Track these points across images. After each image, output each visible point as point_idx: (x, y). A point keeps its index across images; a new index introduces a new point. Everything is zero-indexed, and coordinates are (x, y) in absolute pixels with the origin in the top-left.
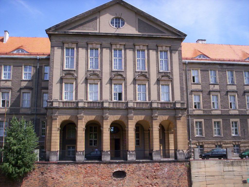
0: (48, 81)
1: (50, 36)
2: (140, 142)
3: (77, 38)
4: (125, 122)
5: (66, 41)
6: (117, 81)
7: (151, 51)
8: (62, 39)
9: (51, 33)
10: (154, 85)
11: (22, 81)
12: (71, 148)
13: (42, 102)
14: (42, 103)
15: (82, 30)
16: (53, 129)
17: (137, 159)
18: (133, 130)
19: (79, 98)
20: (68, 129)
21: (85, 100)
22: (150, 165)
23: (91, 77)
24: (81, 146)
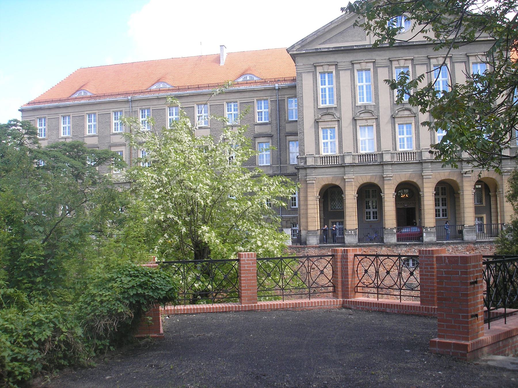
0: (296, 121)
1: (294, 57)
2: (449, 212)
3: (336, 56)
4: (419, 183)
5: (318, 63)
6: (403, 119)
7: (456, 65)
8: (313, 60)
9: (295, 52)
10: (311, 127)
11: (256, 125)
12: (337, 223)
13: (288, 155)
14: (288, 158)
15: (342, 42)
16: (309, 198)
17: (437, 239)
18: (432, 195)
19: (345, 150)
20: (331, 196)
21: (354, 152)
22: (460, 249)
23: (362, 115)
24: (352, 221)
